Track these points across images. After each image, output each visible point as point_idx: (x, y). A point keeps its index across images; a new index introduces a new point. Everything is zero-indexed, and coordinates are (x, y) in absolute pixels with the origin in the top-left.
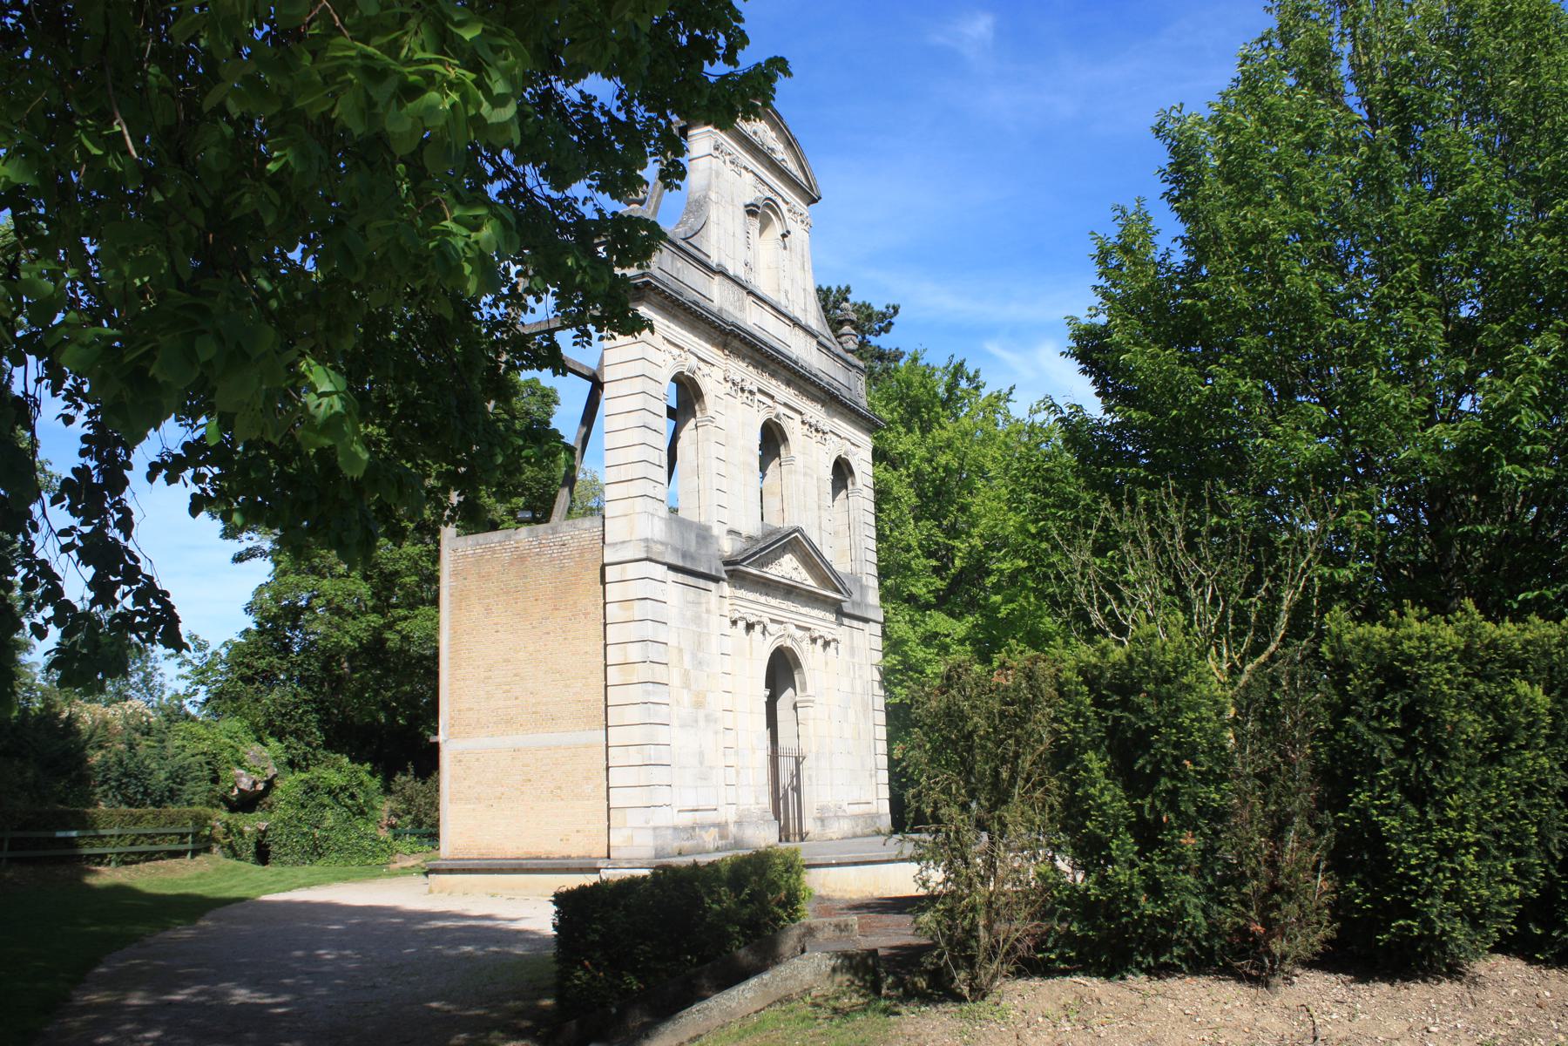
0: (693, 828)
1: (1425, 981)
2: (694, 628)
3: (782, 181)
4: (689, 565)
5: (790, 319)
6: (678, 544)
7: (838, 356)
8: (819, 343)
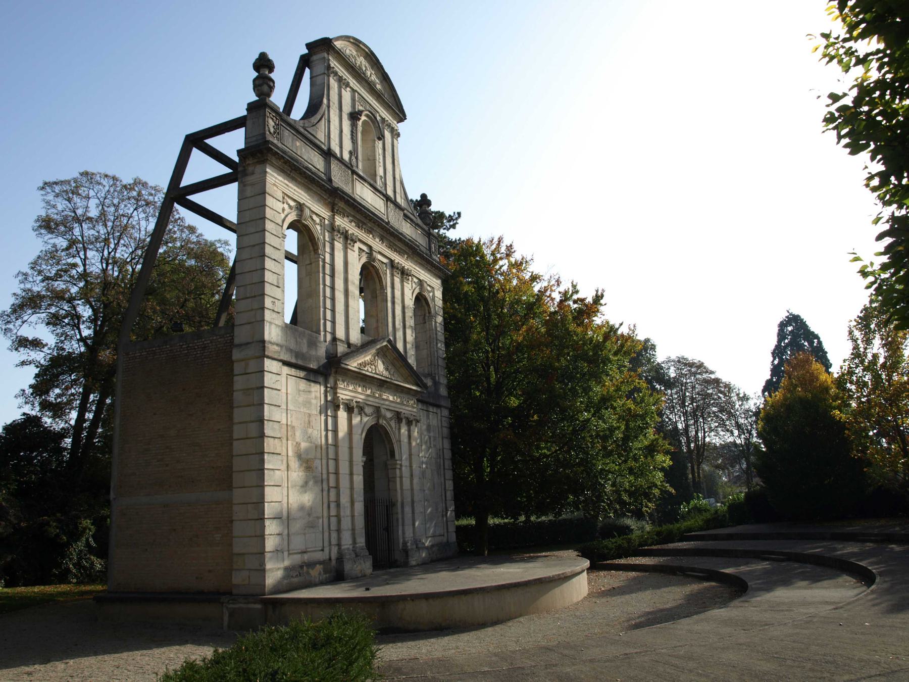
0: (301, 567)
1: (301, 465)
2: (305, 410)
3: (379, 102)
4: (300, 362)
5: (286, 162)
6: (293, 346)
7: (417, 225)
8: (405, 215)
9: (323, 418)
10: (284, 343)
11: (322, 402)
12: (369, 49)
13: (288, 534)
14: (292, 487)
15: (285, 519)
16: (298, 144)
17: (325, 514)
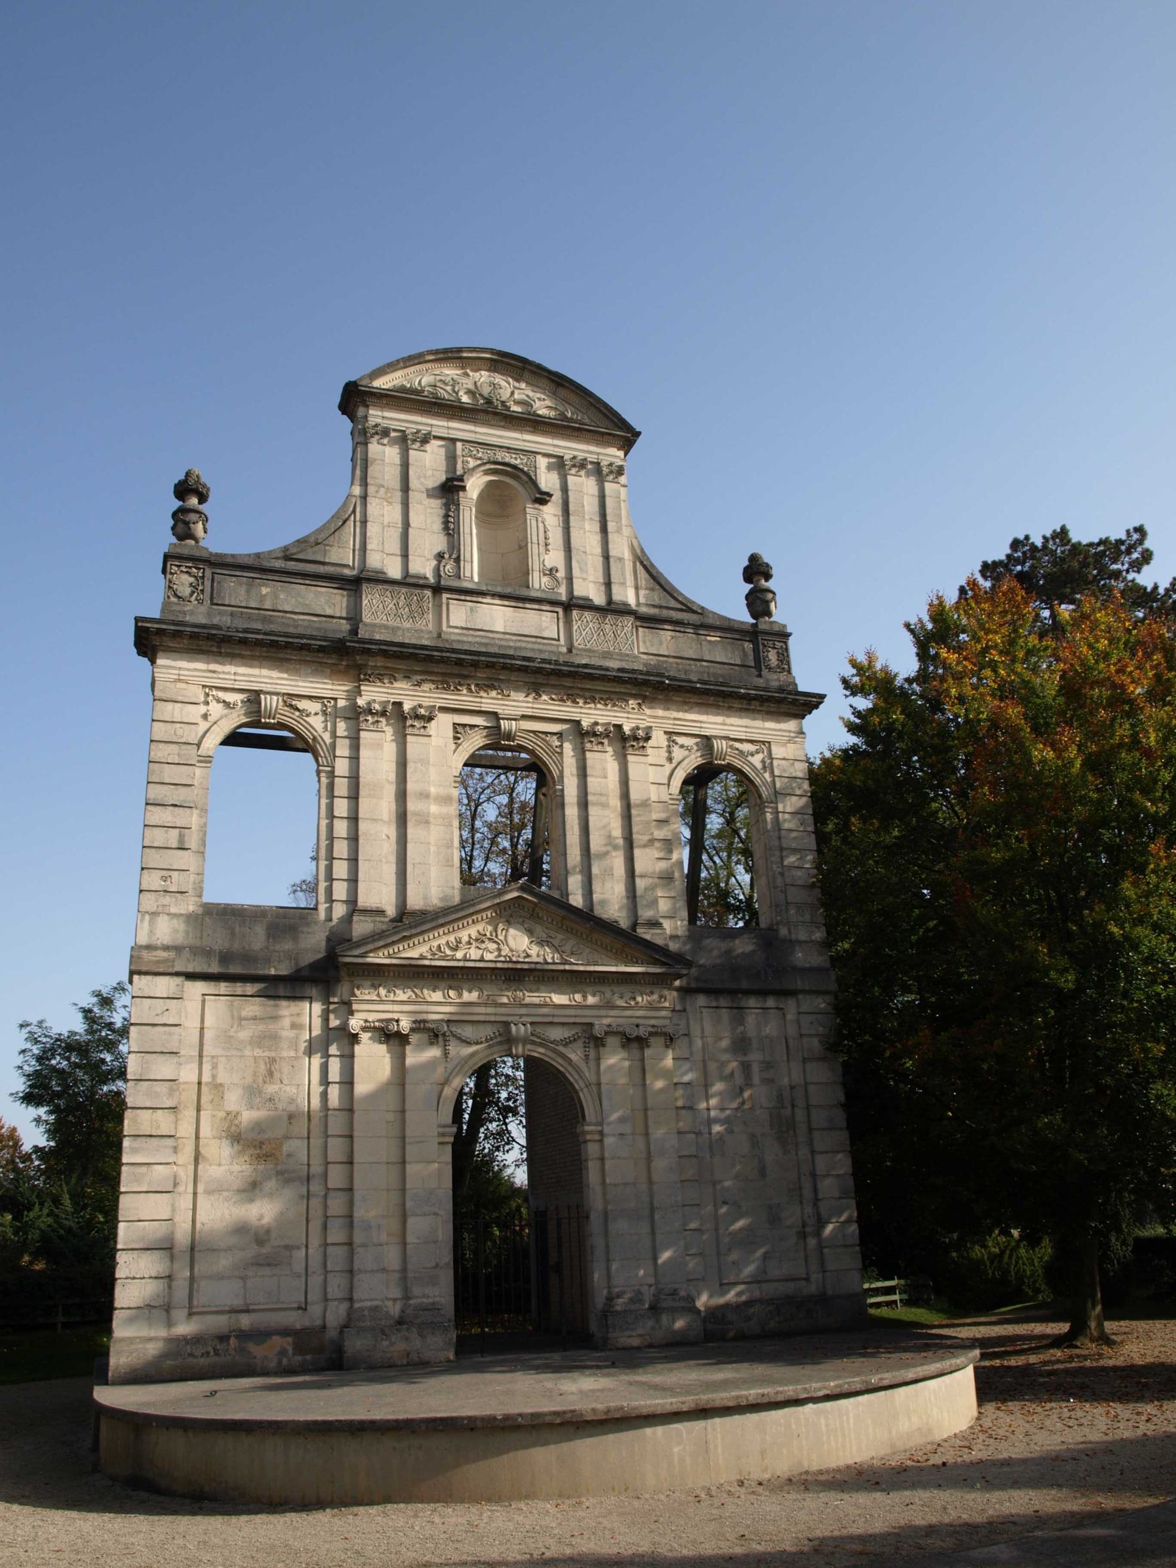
9: (317, 1060)
10: (191, 941)
11: (317, 1031)
12: (492, 351)
13: (192, 1279)
14: (209, 1192)
15: (184, 1254)
16: (264, 590)
17: (315, 1241)
